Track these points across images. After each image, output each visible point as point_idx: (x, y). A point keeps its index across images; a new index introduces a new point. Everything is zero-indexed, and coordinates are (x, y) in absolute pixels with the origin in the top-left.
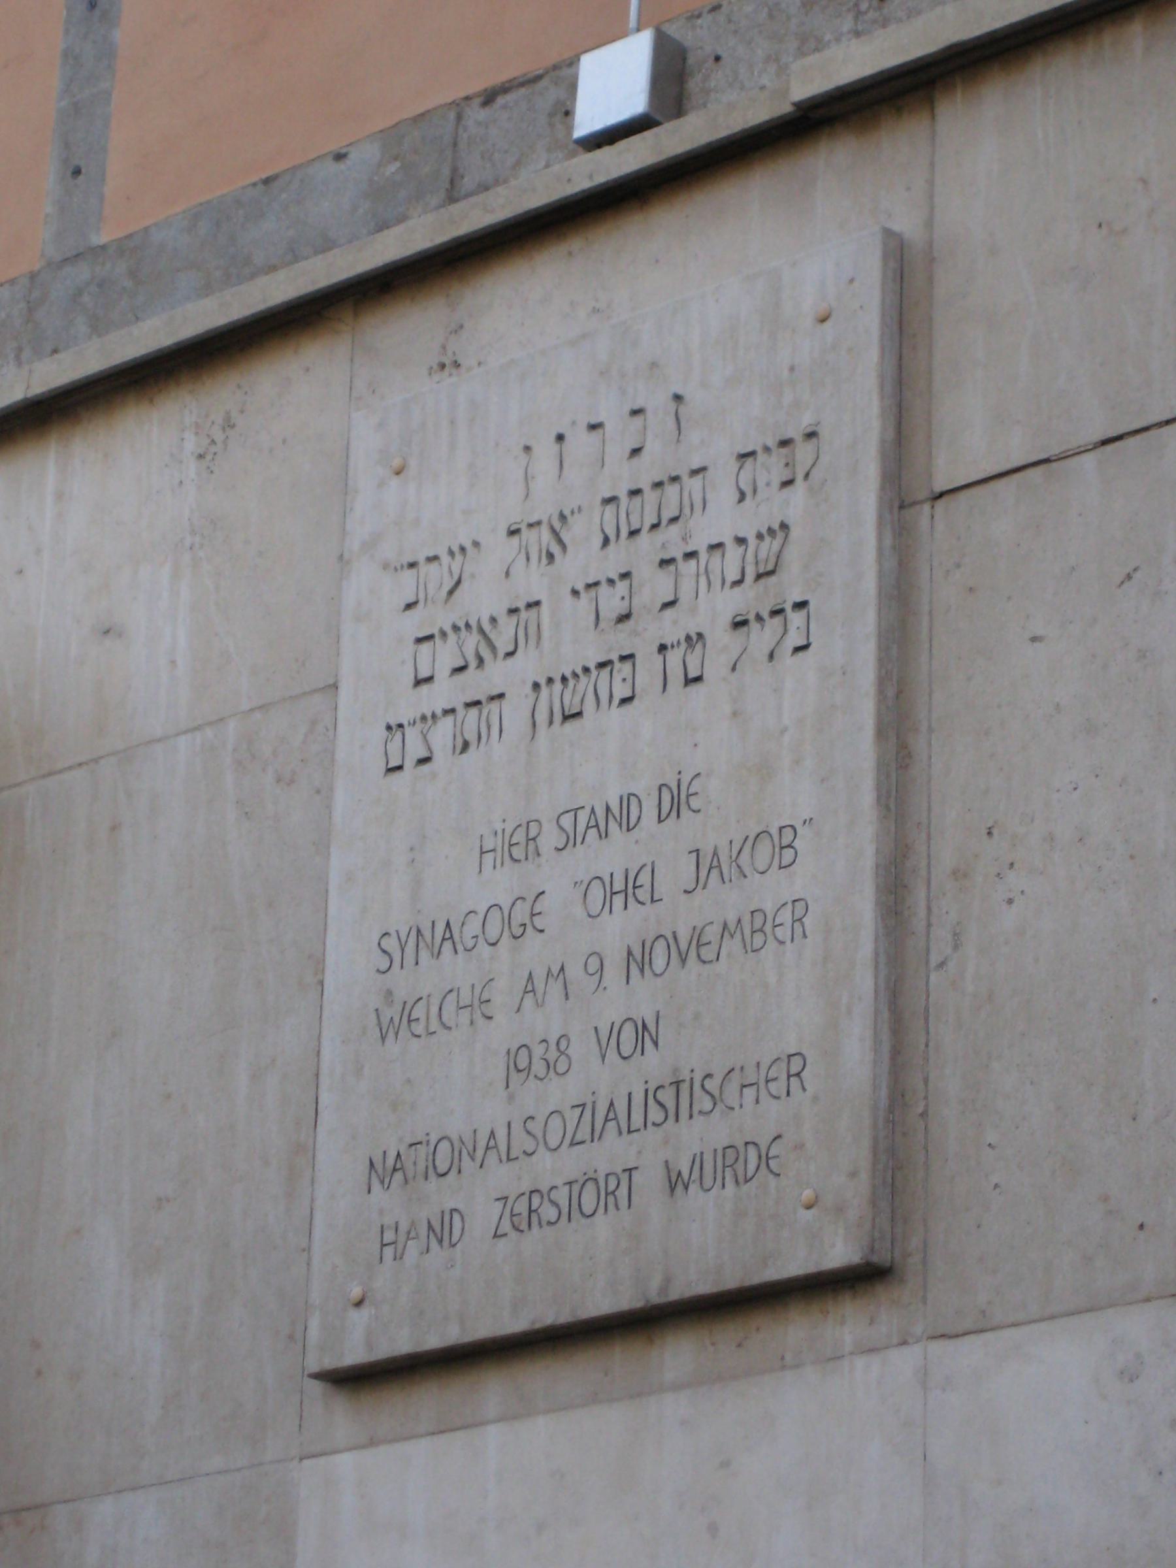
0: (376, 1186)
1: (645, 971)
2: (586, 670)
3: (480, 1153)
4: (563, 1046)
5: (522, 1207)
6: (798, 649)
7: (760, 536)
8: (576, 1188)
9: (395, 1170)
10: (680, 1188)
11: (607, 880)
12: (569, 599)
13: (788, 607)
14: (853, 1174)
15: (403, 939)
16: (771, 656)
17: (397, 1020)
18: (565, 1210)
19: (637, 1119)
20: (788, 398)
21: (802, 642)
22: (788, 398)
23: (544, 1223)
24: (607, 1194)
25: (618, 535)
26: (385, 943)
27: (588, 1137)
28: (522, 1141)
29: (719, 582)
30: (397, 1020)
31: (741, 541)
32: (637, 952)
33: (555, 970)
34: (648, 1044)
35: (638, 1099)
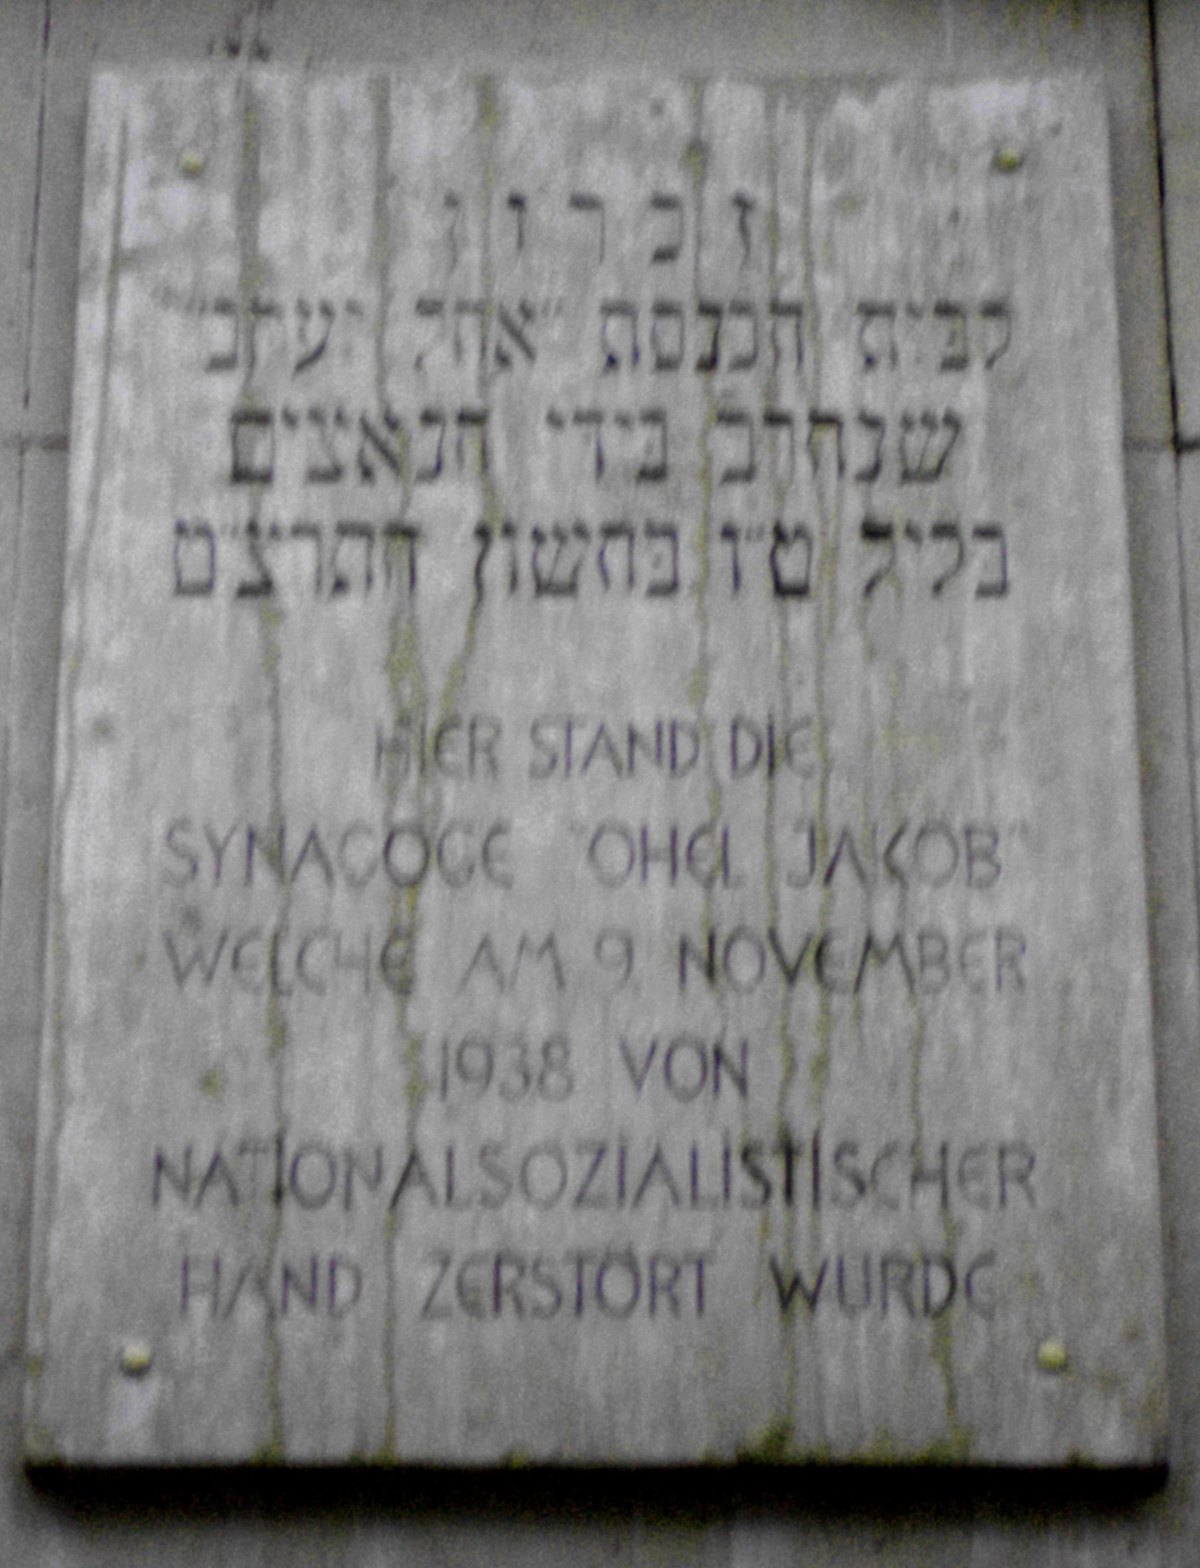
0: (169, 1196)
1: (647, 1157)
2: (581, 531)
3: (390, 1182)
4: (556, 1053)
5: (482, 1276)
6: (984, 592)
7: (907, 423)
8: (590, 1271)
9: (209, 1178)
10: (799, 1303)
11: (637, 836)
12: (543, 434)
13: (967, 531)
14: (1133, 1335)
15: (640, 1065)
16: (938, 588)
17: (209, 957)
18: (569, 1290)
19: (710, 1183)
20: (948, 253)
21: (994, 577)
22: (948, 253)
23: (528, 1308)
24: (653, 1288)
25: (636, 355)
26: (180, 837)
27: (612, 1189)
28: (469, 1179)
29: (833, 466)
30: (209, 957)
31: (871, 422)
32: (700, 944)
33: (537, 940)
34: (726, 1081)
35: (711, 1159)
